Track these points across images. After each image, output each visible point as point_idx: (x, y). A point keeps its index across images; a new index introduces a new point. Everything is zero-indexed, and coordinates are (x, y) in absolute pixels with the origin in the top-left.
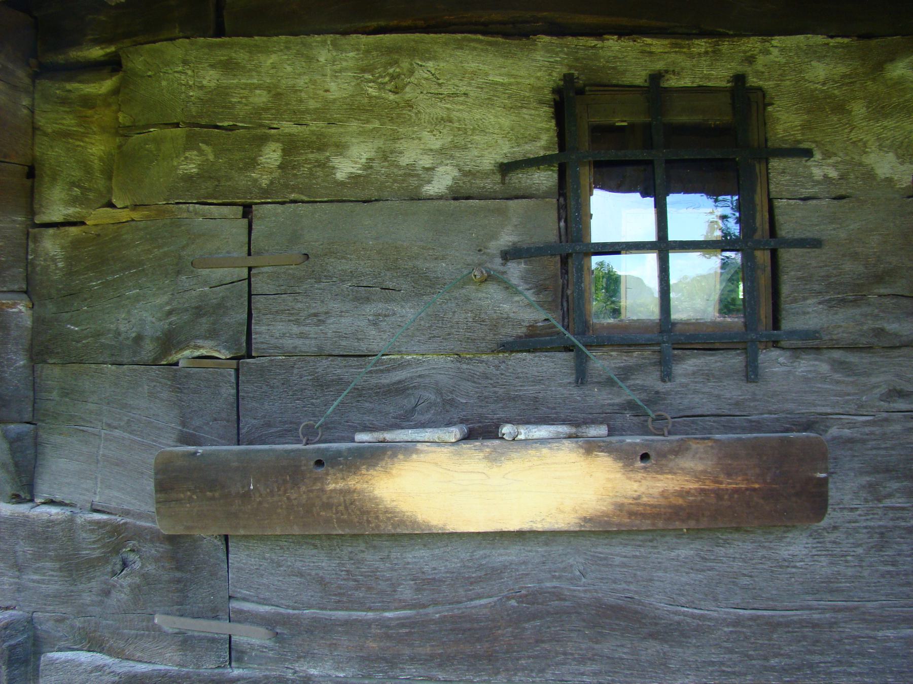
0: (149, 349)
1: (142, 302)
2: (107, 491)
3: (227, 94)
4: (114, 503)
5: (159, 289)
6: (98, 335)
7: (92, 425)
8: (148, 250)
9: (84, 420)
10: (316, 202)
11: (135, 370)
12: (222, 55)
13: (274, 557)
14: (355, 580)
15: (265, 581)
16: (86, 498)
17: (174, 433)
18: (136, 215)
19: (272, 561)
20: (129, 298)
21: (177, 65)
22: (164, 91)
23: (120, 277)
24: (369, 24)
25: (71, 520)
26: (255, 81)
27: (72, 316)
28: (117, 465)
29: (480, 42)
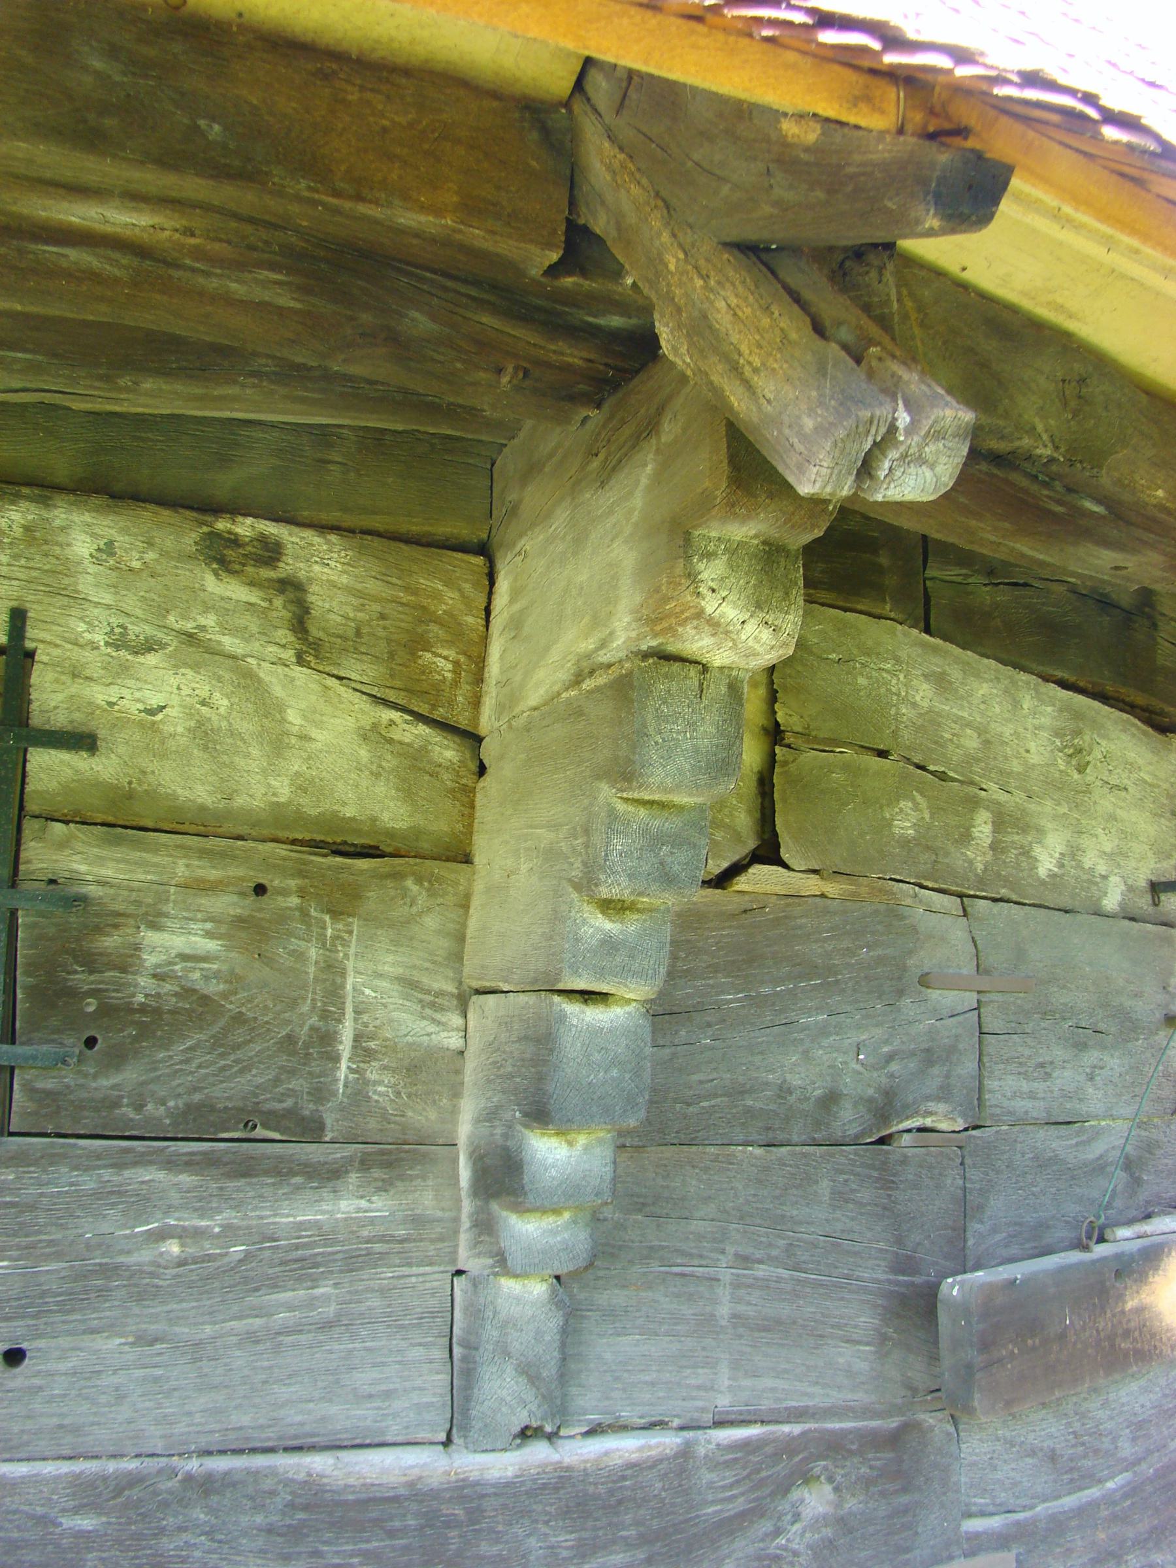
0: (848, 1119)
1: (834, 1037)
2: (747, 1382)
3: (939, 725)
4: (766, 1402)
5: (867, 1017)
6: (738, 1091)
7: (704, 1262)
8: (848, 949)
9: (683, 1253)
10: (1025, 904)
11: (804, 1155)
12: (936, 664)
13: (1008, 1434)
14: (1083, 1444)
15: (999, 1475)
16: (700, 1404)
17: (885, 1259)
18: (831, 888)
19: (1006, 1441)
20: (806, 1028)
21: (886, 660)
22: (862, 694)
23: (789, 991)
24: (1056, 673)
25: (685, 1453)
26: (965, 714)
27: (674, 1054)
28: (766, 1329)
29: (1138, 728)
